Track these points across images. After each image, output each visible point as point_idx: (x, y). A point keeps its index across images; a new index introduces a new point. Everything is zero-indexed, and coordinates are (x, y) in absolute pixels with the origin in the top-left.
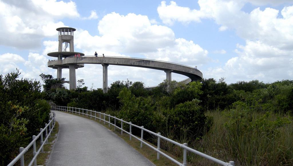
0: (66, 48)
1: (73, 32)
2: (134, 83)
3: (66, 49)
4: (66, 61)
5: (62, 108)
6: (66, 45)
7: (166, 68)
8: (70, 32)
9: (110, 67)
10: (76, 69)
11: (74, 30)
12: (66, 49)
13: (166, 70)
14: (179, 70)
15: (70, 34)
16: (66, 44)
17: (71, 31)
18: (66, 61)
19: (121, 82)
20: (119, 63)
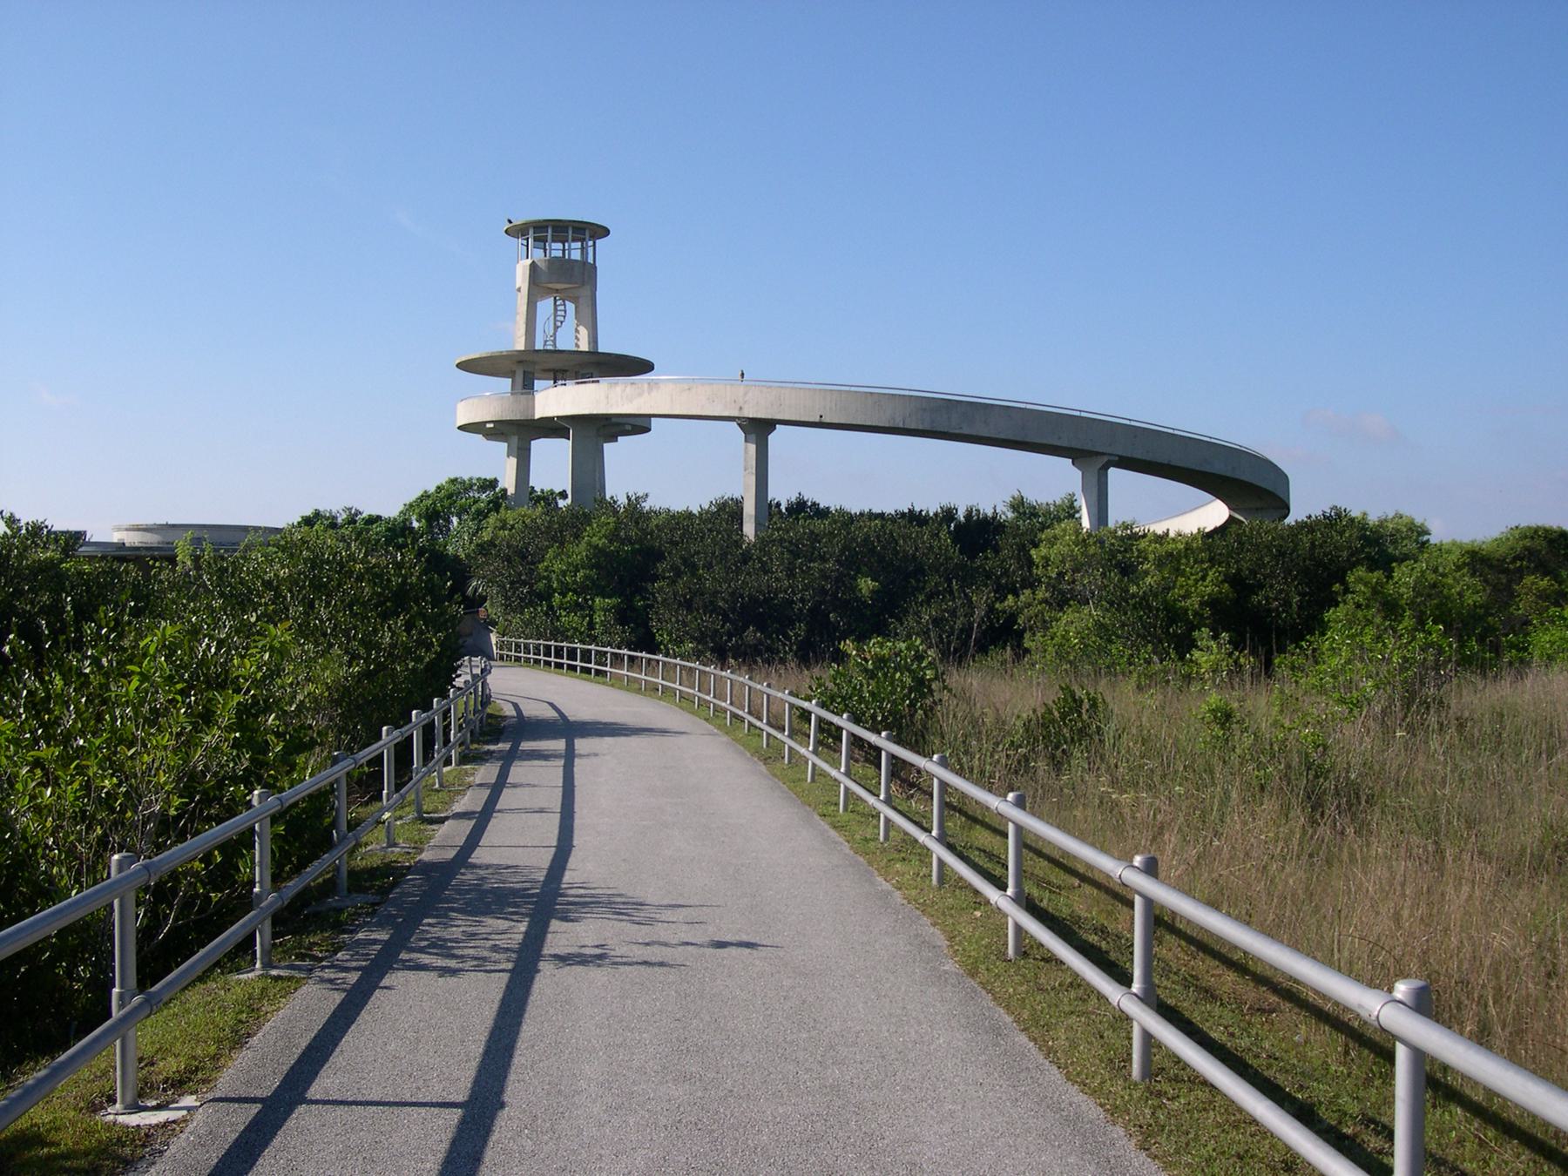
0: (556, 328)
1: (594, 243)
2: (1302, 517)
3: (555, 334)
4: (554, 400)
5: (527, 647)
6: (556, 316)
7: (1075, 444)
8: (579, 245)
9: (777, 438)
10: (606, 446)
11: (605, 232)
12: (555, 334)
13: (1077, 455)
14: (1148, 457)
15: (576, 255)
16: (556, 310)
17: (583, 240)
18: (554, 400)
19: (939, 510)
20: (827, 419)
